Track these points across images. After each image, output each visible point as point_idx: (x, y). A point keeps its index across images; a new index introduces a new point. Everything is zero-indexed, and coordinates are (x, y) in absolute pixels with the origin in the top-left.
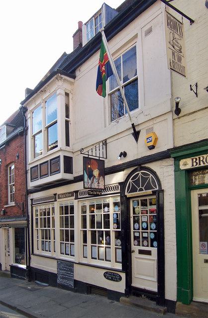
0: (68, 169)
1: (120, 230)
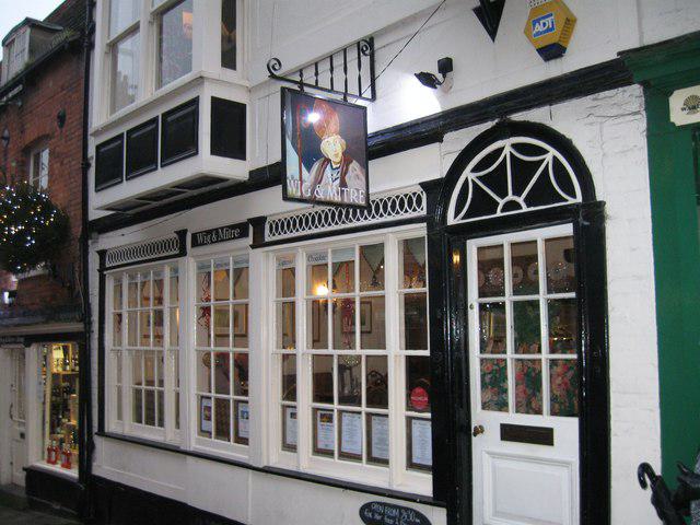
0: (230, 137)
1: (427, 353)
